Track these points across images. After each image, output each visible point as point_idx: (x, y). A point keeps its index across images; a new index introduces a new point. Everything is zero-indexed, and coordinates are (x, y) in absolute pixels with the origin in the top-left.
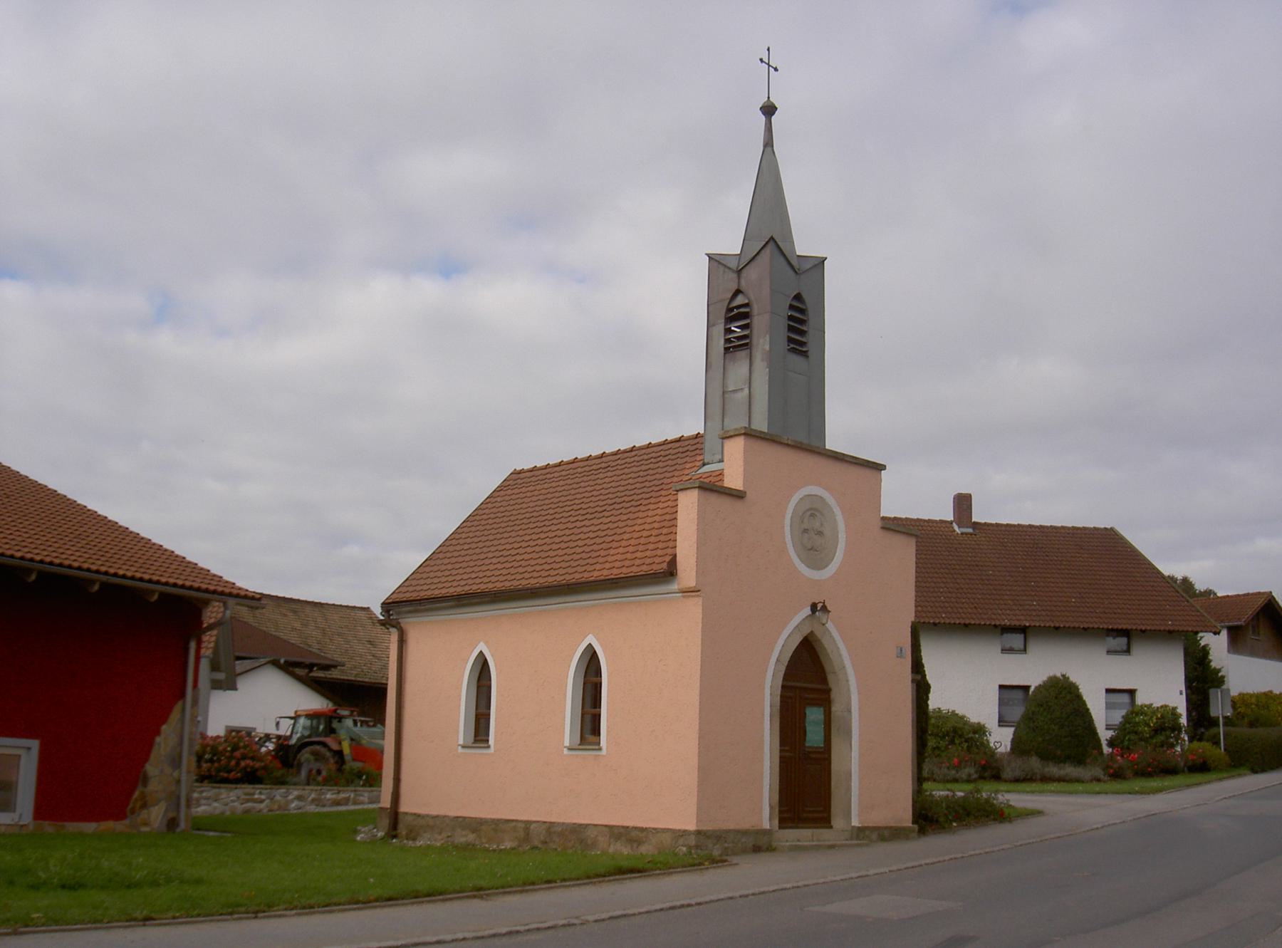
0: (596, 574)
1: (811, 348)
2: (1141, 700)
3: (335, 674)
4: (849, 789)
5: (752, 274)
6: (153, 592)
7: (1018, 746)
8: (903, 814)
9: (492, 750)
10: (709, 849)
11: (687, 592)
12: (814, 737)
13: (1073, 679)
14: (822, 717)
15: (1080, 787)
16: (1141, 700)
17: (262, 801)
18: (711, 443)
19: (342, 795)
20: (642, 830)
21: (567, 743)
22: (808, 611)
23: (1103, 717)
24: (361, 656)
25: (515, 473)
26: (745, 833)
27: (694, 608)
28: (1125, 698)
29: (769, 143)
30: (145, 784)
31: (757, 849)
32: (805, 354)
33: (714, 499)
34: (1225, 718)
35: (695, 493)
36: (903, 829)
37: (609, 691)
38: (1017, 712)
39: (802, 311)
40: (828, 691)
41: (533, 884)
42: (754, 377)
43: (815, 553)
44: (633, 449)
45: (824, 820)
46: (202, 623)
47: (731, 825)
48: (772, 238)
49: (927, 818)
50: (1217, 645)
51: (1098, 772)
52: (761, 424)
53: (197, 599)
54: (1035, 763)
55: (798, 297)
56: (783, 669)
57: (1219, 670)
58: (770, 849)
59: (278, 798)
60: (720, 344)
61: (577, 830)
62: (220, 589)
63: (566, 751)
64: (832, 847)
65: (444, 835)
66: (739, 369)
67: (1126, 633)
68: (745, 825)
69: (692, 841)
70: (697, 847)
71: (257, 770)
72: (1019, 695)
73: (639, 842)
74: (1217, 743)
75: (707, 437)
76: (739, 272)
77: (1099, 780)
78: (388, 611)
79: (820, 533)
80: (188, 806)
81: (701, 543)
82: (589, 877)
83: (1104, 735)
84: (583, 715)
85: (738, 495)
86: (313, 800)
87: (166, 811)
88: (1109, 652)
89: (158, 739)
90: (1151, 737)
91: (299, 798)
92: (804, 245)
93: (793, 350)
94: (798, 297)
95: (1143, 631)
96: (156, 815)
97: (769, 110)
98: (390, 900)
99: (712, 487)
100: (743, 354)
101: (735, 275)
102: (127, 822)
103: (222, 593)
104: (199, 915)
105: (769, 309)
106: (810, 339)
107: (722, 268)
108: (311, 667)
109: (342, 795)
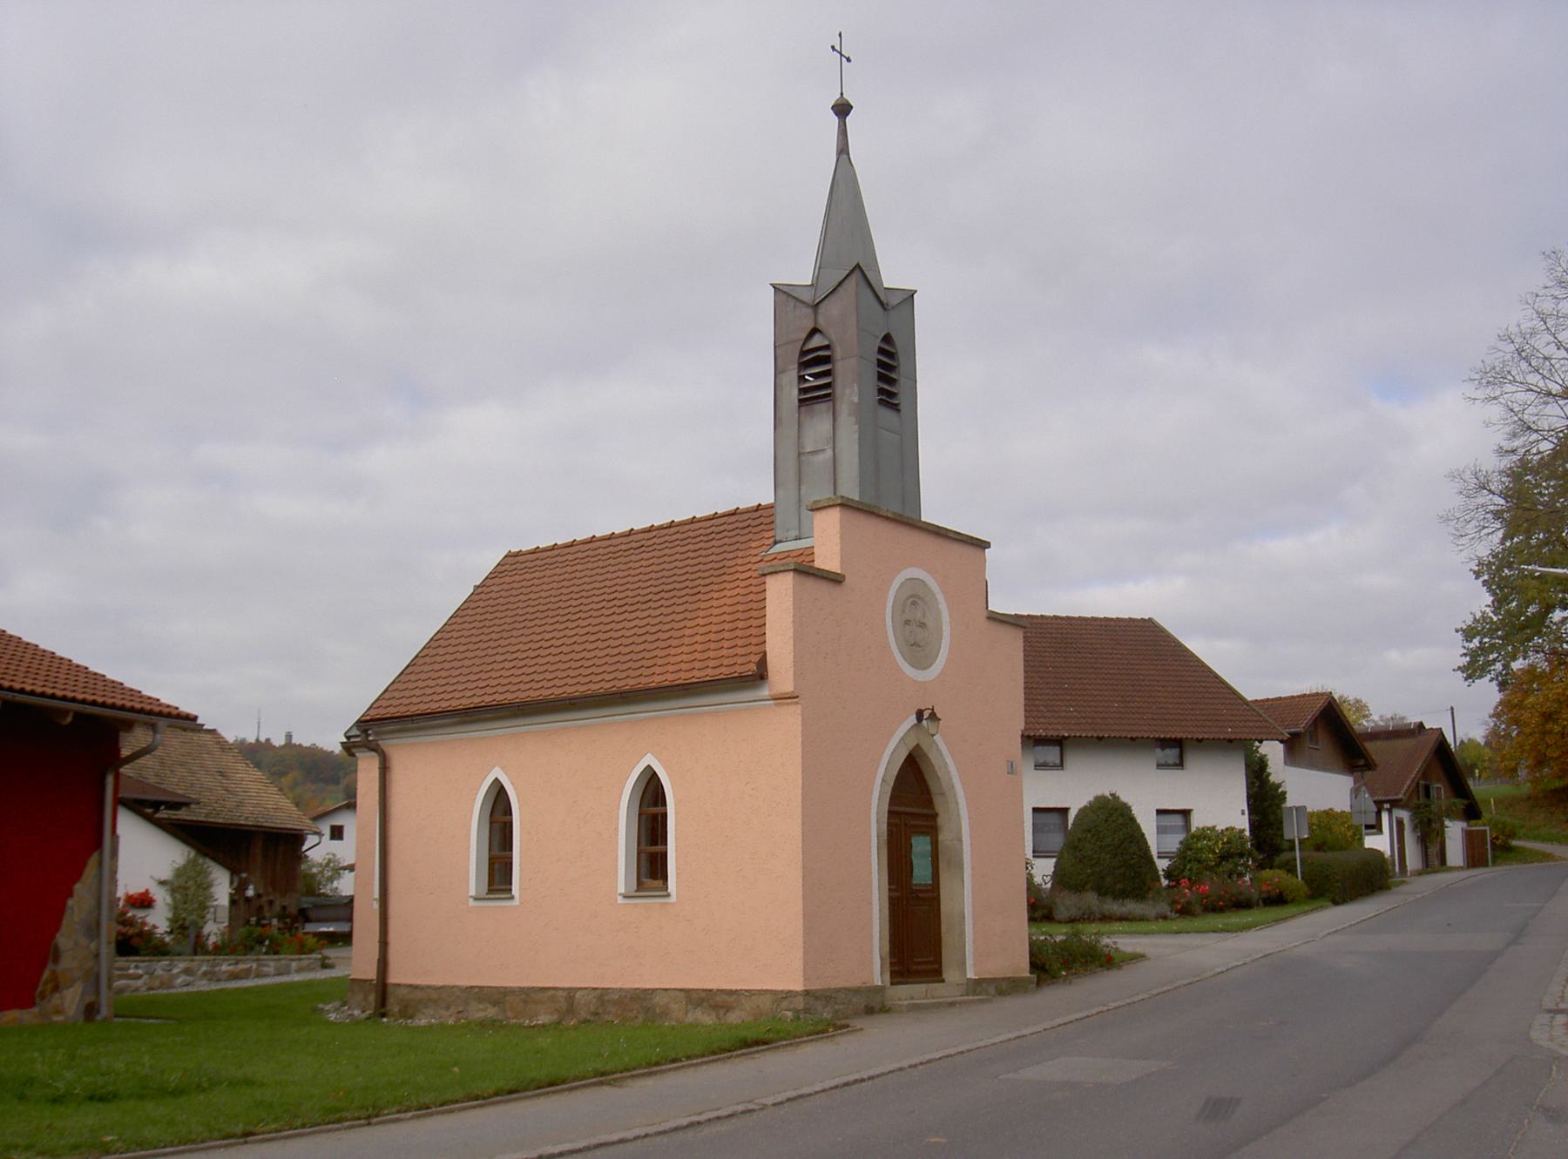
0: (658, 679)
1: (902, 400)
2: (1197, 822)
3: (182, 814)
4: (963, 933)
5: (833, 311)
6: (67, 712)
7: (1059, 877)
8: (1020, 965)
9: (516, 902)
10: (823, 1014)
11: (781, 699)
12: (921, 874)
13: (1124, 798)
14: (929, 848)
15: (1142, 926)
16: (1197, 822)
17: (140, 977)
18: (784, 521)
19: (241, 966)
20: (731, 992)
21: (621, 889)
22: (913, 719)
23: (1160, 844)
24: (210, 790)
25: (509, 555)
26: (856, 991)
27: (791, 717)
28: (1178, 821)
29: (843, 149)
30: (56, 960)
31: (870, 1011)
32: (895, 408)
33: (811, 584)
34: (1301, 842)
35: (790, 576)
36: (1022, 979)
37: (677, 823)
38: (1056, 841)
39: (891, 355)
40: (935, 816)
41: (657, 1064)
42: (840, 433)
43: (919, 649)
44: (672, 524)
45: (934, 972)
46: (118, 751)
47: (841, 983)
48: (858, 266)
49: (1046, 967)
50: (1273, 751)
51: (1164, 907)
52: (850, 490)
53: (116, 719)
54: (1091, 899)
55: (887, 339)
56: (889, 790)
57: (1279, 786)
58: (885, 1010)
59: (159, 972)
60: (793, 394)
61: (641, 997)
62: (138, 706)
63: (620, 900)
64: (952, 1004)
65: (452, 1010)
66: (819, 425)
67: (1178, 744)
68: (854, 982)
69: (800, 1003)
70: (807, 1010)
71: (131, 937)
72: (1054, 819)
73: (728, 1008)
74: (1291, 869)
75: (778, 509)
76: (816, 306)
77: (1165, 918)
78: (365, 731)
79: (923, 625)
80: (110, 980)
81: (798, 638)
82: (714, 1053)
83: (1162, 865)
84: (639, 854)
85: (835, 579)
86: (205, 974)
87: (83, 994)
88: (1159, 766)
89: (70, 902)
90: (1218, 865)
91: (187, 971)
92: (892, 275)
93: (881, 402)
94: (887, 339)
95: (1200, 741)
96: (71, 999)
97: (842, 109)
98: (511, 1092)
99: (805, 570)
100: (823, 407)
101: (810, 311)
102: (36, 1010)
103: (150, 713)
104: (303, 1126)
105: (847, 354)
106: (901, 388)
107: (792, 303)
108: (156, 805)
109: (241, 966)
